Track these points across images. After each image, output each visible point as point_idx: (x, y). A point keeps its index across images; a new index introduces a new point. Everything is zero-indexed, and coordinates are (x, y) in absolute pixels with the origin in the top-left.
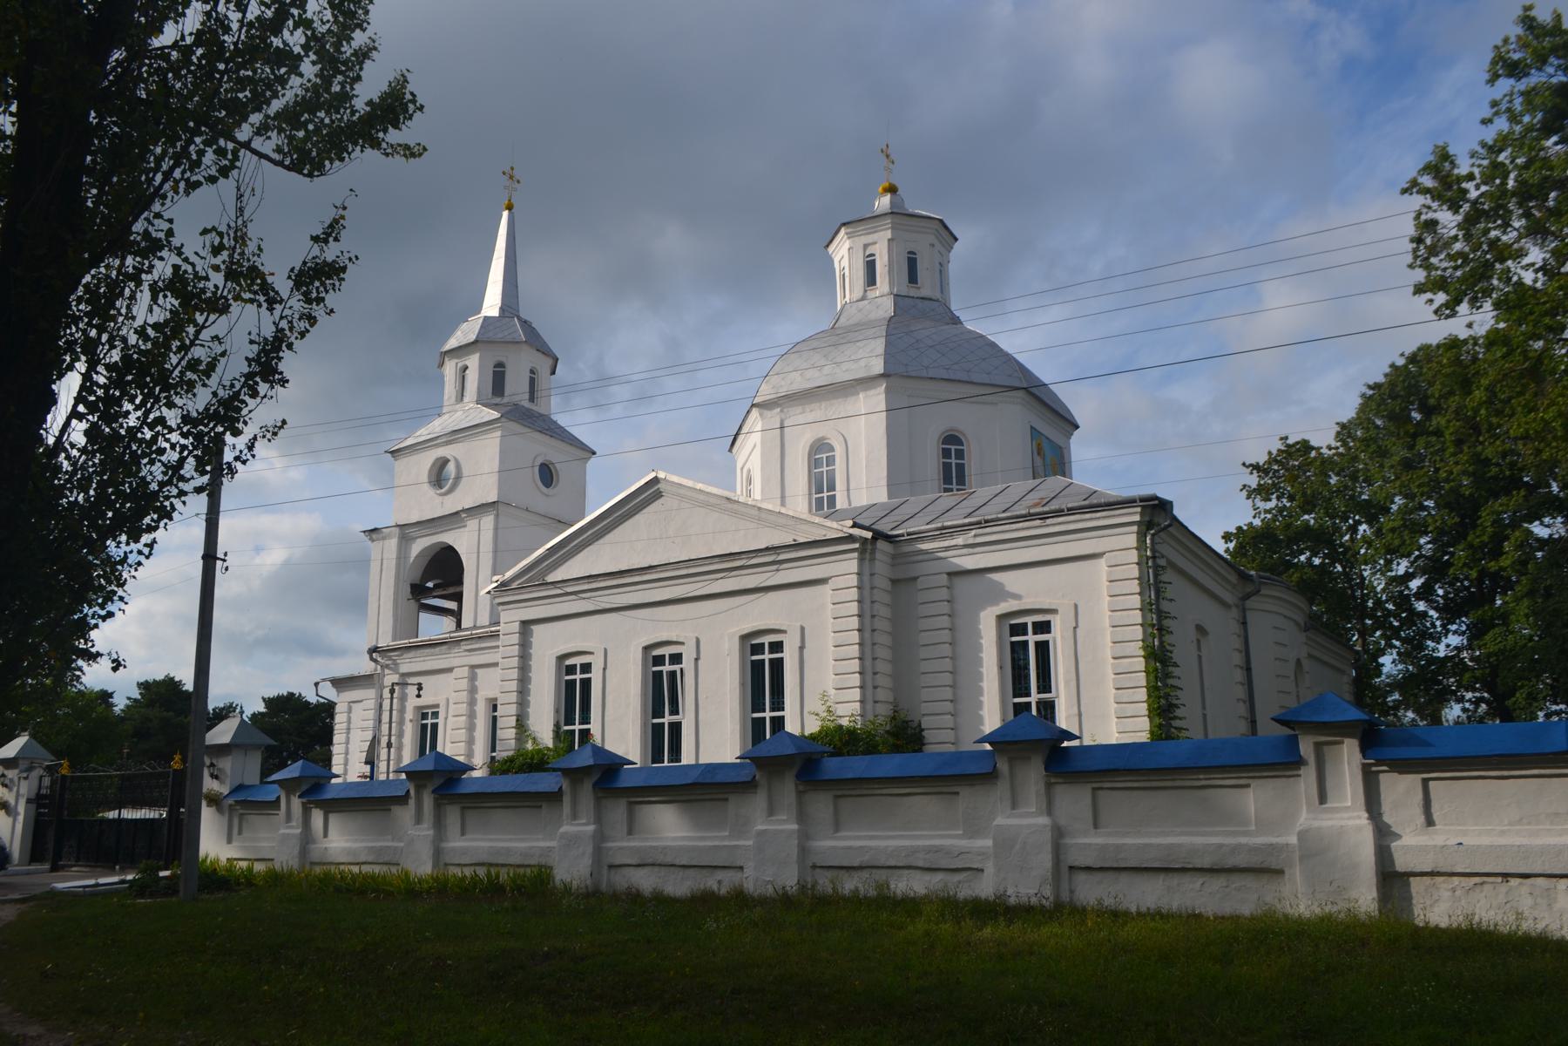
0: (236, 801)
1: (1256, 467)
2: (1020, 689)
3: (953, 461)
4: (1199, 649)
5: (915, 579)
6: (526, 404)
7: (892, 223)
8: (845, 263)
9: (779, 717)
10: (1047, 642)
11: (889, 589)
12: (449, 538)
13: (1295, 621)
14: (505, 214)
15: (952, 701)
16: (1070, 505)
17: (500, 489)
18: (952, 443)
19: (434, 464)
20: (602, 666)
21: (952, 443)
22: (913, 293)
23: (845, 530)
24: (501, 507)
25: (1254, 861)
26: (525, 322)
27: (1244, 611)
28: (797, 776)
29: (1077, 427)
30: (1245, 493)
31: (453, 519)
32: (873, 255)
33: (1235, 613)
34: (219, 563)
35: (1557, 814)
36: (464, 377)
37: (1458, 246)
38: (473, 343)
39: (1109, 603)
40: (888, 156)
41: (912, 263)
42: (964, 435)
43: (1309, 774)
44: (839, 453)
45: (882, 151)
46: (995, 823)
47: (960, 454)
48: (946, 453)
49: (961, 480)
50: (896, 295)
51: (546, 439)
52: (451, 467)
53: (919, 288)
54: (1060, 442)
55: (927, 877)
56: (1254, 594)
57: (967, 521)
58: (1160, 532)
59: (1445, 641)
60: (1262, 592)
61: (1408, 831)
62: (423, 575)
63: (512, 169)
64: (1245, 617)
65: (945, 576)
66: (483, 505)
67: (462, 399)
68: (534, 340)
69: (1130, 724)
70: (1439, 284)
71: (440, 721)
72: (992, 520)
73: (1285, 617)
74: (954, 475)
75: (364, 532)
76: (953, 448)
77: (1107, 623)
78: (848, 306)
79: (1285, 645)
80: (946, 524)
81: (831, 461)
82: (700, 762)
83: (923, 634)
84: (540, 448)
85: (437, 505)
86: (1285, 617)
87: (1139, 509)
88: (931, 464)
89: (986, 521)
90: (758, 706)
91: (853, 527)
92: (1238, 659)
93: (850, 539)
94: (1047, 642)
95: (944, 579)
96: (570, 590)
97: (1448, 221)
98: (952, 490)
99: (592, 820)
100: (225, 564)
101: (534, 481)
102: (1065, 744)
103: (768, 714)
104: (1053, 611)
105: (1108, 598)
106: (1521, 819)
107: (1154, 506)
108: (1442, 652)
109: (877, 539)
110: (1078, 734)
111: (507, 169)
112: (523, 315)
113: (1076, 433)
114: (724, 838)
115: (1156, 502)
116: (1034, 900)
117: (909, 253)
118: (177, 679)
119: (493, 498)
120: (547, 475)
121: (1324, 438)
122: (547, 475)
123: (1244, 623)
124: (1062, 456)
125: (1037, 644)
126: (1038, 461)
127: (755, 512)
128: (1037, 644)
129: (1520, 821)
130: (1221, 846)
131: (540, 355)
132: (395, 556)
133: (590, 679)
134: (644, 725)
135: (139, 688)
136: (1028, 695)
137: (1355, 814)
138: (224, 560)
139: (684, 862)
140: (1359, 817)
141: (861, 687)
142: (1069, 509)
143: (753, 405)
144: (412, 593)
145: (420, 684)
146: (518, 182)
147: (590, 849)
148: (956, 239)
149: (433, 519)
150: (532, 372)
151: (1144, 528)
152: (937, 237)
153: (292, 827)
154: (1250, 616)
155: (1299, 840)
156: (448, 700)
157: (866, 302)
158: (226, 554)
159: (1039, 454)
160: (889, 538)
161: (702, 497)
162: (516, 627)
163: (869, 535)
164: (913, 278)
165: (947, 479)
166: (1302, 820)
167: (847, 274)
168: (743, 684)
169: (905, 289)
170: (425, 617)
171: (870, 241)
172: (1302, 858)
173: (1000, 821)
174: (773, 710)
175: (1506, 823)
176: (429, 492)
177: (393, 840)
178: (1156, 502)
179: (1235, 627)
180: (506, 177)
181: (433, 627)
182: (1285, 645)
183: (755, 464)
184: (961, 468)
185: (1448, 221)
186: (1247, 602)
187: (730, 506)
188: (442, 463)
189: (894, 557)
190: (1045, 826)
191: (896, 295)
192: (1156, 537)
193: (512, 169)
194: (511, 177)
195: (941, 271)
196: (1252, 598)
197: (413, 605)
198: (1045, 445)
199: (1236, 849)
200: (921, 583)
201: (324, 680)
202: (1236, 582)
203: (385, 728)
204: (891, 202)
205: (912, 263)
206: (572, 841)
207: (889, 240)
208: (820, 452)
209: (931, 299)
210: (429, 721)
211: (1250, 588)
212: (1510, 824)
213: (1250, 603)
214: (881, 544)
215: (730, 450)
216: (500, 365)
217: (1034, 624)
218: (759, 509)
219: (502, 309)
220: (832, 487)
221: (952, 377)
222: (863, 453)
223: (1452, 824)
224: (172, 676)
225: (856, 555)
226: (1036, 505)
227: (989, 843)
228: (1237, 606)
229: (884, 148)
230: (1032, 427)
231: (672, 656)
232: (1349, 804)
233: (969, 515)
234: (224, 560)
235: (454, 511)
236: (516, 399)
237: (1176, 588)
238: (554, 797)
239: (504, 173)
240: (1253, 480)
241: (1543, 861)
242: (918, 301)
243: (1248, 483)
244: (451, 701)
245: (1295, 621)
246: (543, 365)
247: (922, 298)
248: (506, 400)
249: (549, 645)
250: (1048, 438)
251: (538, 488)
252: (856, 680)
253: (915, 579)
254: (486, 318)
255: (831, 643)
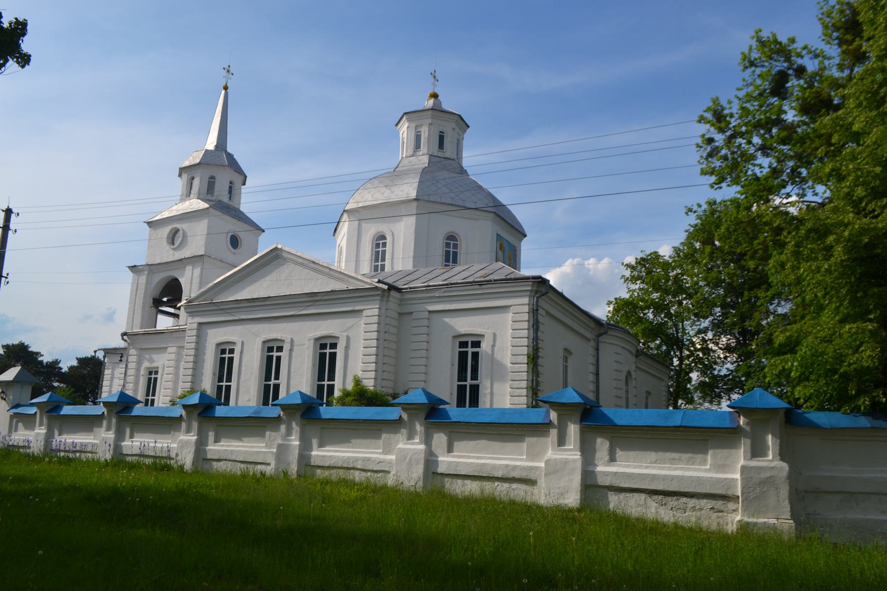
0: (14, 413)
1: (628, 266)
2: (462, 377)
3: (451, 250)
4: (566, 362)
5: (412, 313)
6: (226, 199)
7: (432, 115)
8: (405, 135)
9: (332, 385)
10: (478, 352)
11: (397, 317)
12: (175, 274)
13: (629, 351)
14: (223, 92)
15: (425, 381)
16: (495, 278)
17: (206, 248)
18: (451, 239)
19: (170, 232)
20: (240, 351)
21: (451, 239)
22: (440, 154)
23: (374, 283)
24: (205, 258)
25: (523, 475)
26: (229, 154)
27: (598, 343)
28: (301, 416)
29: (525, 236)
30: (623, 280)
31: (182, 262)
32: (420, 132)
33: (592, 343)
34: (3, 279)
35: (674, 459)
36: (192, 183)
37: (723, 152)
38: (199, 164)
39: (511, 333)
40: (434, 77)
41: (441, 138)
42: (459, 236)
43: (554, 432)
44: (389, 241)
45: (431, 74)
46: (398, 447)
47: (455, 246)
48: (448, 245)
49: (455, 261)
50: (430, 155)
51: (235, 221)
52: (180, 234)
53: (444, 152)
54: (513, 241)
55: (363, 474)
56: (604, 334)
57: (423, 285)
58: (541, 296)
59: (726, 366)
60: (609, 333)
61: (600, 463)
62: (160, 294)
63: (229, 66)
64: (598, 346)
65: (427, 313)
66: (195, 256)
67: (189, 196)
68: (233, 163)
69: (517, 400)
70: (712, 172)
71: (159, 376)
72: (454, 284)
73: (623, 348)
74: (451, 258)
75: (129, 267)
76: (452, 242)
77: (509, 344)
78: (404, 159)
79: (621, 363)
80: (430, 284)
81: (384, 245)
82: (495, 406)
83: (413, 344)
84: (231, 225)
85: (168, 254)
86: (623, 348)
87: (531, 283)
88: (438, 249)
89: (451, 284)
90: (220, 379)
91: (377, 282)
92: (592, 368)
93: (376, 288)
94: (478, 352)
95: (426, 315)
96: (221, 307)
97: (720, 138)
98: (449, 266)
99: (196, 434)
100: (7, 280)
101: (227, 245)
102: (441, 407)
103: (326, 383)
104: (483, 336)
105: (511, 331)
106: (656, 461)
107: (539, 282)
108: (724, 372)
109: (391, 290)
110: (448, 401)
111: (226, 67)
112: (229, 150)
113: (525, 239)
114: (262, 447)
115: (540, 280)
116: (412, 489)
117: (440, 132)
118: (26, 344)
119: (202, 252)
120: (235, 242)
121: (666, 252)
122: (235, 242)
123: (597, 350)
124: (515, 251)
125: (473, 353)
126: (500, 253)
127: (327, 270)
128: (473, 353)
129: (655, 462)
130: (507, 466)
131: (236, 173)
132: (145, 282)
133: (233, 357)
134: (260, 384)
135: (3, 348)
136: (466, 381)
137: (574, 453)
138: (7, 278)
139: (241, 459)
140: (576, 455)
141: (376, 371)
142: (495, 281)
143: (344, 211)
144: (153, 303)
145: (122, 354)
146: (232, 74)
147: (193, 450)
148: (468, 127)
149: (168, 262)
150: (231, 183)
151: (533, 294)
152: (457, 125)
153: (42, 429)
154: (601, 346)
155: (545, 464)
156: (164, 365)
157: (413, 158)
158: (8, 274)
159: (501, 249)
160: (399, 290)
161: (300, 260)
162: (195, 326)
163: (386, 287)
164: (441, 145)
165: (447, 260)
166: (548, 455)
167: (405, 141)
168: (314, 365)
169: (435, 151)
170: (160, 317)
171: (419, 124)
172: (546, 475)
173: (401, 446)
174: (329, 380)
175: (649, 462)
176: (168, 247)
177: (94, 439)
178: (540, 280)
179: (591, 351)
180: (225, 71)
181: (164, 322)
182: (621, 363)
183: (344, 244)
184: (455, 254)
185: (720, 138)
186: (600, 338)
187: (314, 266)
188: (176, 231)
189: (401, 300)
190: (422, 450)
191: (430, 155)
192: (539, 299)
193: (229, 66)
194: (228, 71)
195: (458, 144)
196: (603, 336)
197: (154, 310)
198: (505, 245)
199: (494, 467)
200: (414, 316)
201: (99, 350)
202: (593, 326)
203: (130, 379)
204: (434, 103)
205: (441, 138)
206: (183, 444)
207: (430, 124)
208: (380, 240)
209: (450, 159)
210: (153, 376)
211: (602, 331)
212: (650, 463)
213: (601, 339)
214: (393, 293)
215: (334, 235)
216: (212, 177)
217: (472, 342)
218: (330, 269)
219: (216, 146)
220: (383, 259)
221: (454, 203)
222: (402, 242)
223: (622, 461)
224: (23, 342)
225: (378, 298)
226: (481, 277)
227: (393, 457)
228: (595, 340)
229: (433, 72)
230: (497, 234)
231: (331, 344)
232: (572, 447)
233: (445, 280)
234: (7, 278)
235: (179, 258)
236: (221, 198)
237: (547, 324)
238: (278, 419)
239: (224, 69)
240: (628, 273)
241: (664, 484)
242: (443, 160)
243: (625, 274)
244: (166, 366)
245: (629, 351)
246: (237, 179)
247: (446, 158)
248: (213, 198)
249: (215, 336)
250: (507, 241)
251: (229, 250)
252: (373, 367)
253: (412, 313)
254: (207, 151)
255: (362, 345)
